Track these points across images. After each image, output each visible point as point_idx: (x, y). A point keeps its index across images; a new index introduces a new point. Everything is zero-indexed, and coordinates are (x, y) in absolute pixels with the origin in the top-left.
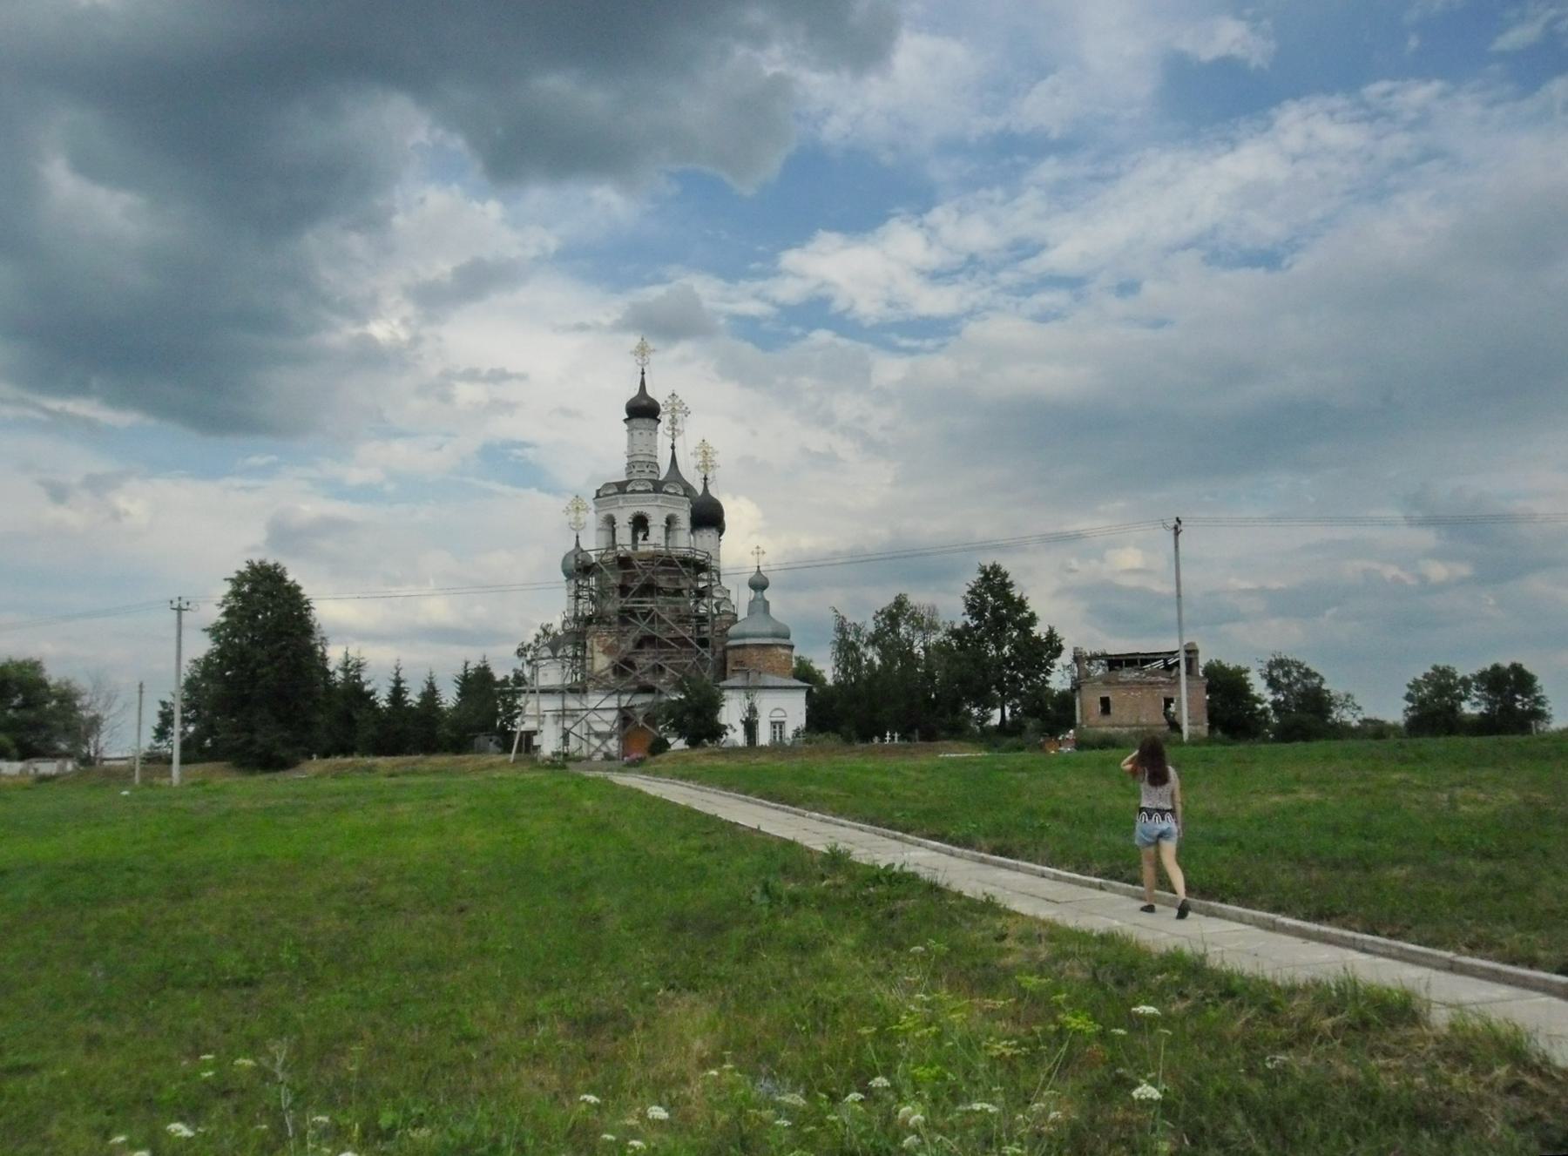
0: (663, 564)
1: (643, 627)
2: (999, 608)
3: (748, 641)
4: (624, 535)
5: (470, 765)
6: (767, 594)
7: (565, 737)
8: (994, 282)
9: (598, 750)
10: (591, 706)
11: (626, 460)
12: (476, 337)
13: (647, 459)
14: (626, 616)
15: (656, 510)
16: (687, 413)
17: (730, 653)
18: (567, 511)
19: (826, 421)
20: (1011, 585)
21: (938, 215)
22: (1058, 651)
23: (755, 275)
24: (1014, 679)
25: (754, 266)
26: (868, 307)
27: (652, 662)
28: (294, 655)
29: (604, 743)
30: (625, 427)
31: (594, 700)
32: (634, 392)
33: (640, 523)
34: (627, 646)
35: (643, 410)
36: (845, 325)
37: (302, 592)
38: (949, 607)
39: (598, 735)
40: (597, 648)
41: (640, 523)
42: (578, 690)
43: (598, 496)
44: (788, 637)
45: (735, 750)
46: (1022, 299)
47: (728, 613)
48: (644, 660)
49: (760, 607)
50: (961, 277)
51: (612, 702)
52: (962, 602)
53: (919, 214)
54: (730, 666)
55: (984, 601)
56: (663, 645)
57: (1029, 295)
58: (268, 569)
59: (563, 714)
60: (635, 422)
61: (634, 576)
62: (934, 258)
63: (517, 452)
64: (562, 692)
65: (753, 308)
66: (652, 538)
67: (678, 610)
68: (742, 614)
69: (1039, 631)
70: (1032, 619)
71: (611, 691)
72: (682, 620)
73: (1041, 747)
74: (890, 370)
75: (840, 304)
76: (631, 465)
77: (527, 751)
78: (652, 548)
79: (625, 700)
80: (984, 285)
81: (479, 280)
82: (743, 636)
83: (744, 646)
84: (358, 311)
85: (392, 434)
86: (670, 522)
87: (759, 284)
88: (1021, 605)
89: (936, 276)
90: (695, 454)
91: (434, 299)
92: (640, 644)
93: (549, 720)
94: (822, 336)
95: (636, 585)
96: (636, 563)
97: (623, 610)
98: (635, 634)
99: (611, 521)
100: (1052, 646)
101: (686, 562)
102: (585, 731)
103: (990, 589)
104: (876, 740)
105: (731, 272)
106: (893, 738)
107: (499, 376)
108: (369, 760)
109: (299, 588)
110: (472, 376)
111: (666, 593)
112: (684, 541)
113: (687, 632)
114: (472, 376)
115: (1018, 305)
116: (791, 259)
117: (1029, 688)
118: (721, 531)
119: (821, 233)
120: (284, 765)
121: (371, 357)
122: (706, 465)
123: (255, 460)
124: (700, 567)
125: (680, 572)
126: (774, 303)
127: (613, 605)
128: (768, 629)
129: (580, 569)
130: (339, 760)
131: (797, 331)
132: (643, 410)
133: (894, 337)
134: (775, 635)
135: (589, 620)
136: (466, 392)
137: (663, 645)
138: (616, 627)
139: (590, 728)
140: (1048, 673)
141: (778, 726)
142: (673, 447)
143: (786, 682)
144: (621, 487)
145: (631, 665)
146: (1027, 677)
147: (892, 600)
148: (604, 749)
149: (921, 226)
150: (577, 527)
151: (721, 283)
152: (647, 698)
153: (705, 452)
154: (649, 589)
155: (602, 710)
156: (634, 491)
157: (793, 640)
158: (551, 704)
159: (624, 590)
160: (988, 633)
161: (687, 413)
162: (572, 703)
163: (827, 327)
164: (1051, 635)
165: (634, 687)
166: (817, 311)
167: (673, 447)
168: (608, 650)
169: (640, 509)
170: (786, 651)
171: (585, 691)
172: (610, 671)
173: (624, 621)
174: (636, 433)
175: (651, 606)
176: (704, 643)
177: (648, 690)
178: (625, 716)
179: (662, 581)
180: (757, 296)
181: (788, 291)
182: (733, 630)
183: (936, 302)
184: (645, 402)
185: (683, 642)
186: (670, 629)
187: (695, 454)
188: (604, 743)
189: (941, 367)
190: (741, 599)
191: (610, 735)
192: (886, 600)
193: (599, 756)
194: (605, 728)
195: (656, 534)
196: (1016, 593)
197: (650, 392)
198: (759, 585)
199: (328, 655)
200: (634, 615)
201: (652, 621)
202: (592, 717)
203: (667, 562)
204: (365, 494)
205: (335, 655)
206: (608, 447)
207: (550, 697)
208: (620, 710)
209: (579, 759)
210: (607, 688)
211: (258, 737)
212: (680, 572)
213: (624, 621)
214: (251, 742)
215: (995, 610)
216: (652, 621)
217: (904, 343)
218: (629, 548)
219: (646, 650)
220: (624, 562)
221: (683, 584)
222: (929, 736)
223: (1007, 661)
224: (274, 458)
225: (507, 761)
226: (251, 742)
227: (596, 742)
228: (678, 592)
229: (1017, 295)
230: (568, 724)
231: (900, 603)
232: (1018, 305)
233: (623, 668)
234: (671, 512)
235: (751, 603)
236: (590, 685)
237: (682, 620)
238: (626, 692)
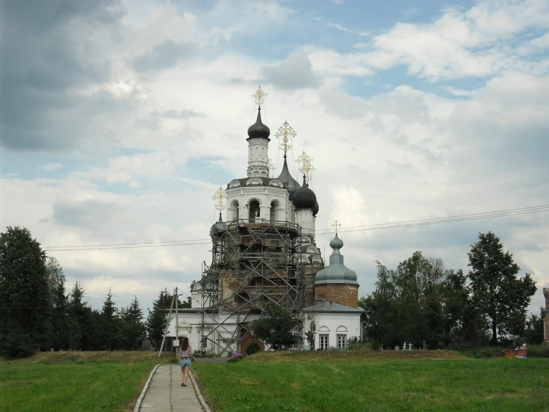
0: (267, 231)
1: (254, 272)
2: (493, 262)
3: (328, 281)
4: (244, 214)
5: (134, 357)
6: (342, 251)
7: (204, 340)
8: (515, 54)
9: (224, 350)
10: (220, 322)
11: (248, 165)
12: (173, 90)
13: (260, 164)
14: (244, 264)
15: (265, 197)
16: (294, 135)
17: (317, 289)
18: (214, 198)
19: (401, 141)
20: (501, 246)
21: (474, 12)
22: (533, 290)
23: (359, 51)
24: (503, 309)
25: (358, 45)
26: (433, 71)
27: (260, 294)
28: (32, 286)
29: (228, 346)
30: (247, 143)
31: (222, 318)
32: (253, 121)
33: (254, 206)
34: (245, 283)
35: (259, 133)
36: (419, 82)
37: (40, 246)
38: (457, 260)
39: (225, 341)
40: (225, 284)
41: (254, 206)
42: (212, 311)
43: (228, 188)
44: (355, 279)
45: (305, 352)
46: (534, 64)
47: (318, 263)
48: (256, 292)
49: (338, 259)
50: (492, 50)
51: (233, 320)
52: (468, 257)
53: (463, 11)
54: (316, 298)
55: (482, 257)
56: (266, 283)
57: (538, 61)
58: (20, 232)
59: (202, 327)
60: (253, 140)
61: (250, 239)
62: (475, 40)
63: (214, 162)
64: (202, 312)
65: (360, 71)
66: (262, 216)
67: (278, 261)
68: (327, 263)
69: (519, 276)
70: (515, 269)
71: (234, 313)
72: (280, 267)
73: (504, 355)
74: (442, 109)
75: (414, 69)
76: (250, 168)
77: (169, 350)
78: (260, 222)
79: (242, 318)
80: (508, 56)
81: (168, 55)
82: (326, 278)
83: (325, 285)
84: (99, 75)
85: (130, 152)
86: (274, 204)
87: (361, 57)
88: (508, 259)
89: (475, 51)
90: (299, 161)
91: (145, 66)
92: (253, 282)
93: (194, 330)
94: (404, 90)
95: (251, 244)
96: (250, 231)
97: (242, 261)
98: (249, 276)
99: (236, 204)
100: (528, 287)
101: (283, 230)
102: (217, 338)
103: (486, 249)
104: (397, 348)
105: (344, 47)
106: (408, 346)
107: (188, 114)
108: (75, 353)
109: (38, 244)
110: (171, 114)
111: (270, 250)
112: (283, 217)
113: (284, 275)
114: (171, 114)
115: (532, 68)
116: (381, 40)
117: (511, 314)
118: (315, 211)
119: (399, 25)
120: (26, 354)
121: (107, 104)
122: (307, 168)
123: (50, 167)
124: (294, 234)
125: (279, 237)
126: (372, 68)
127: (236, 256)
128: (342, 274)
129: (218, 234)
130: (62, 352)
131: (388, 86)
132: (259, 133)
133: (450, 89)
134: (346, 278)
135: (221, 266)
136: (171, 125)
137: (266, 283)
138: (237, 272)
139: (220, 335)
140: (526, 305)
141: (325, 338)
142: (285, 157)
143: (347, 309)
144: (243, 182)
145: (245, 295)
146: (511, 307)
147: (411, 256)
148: (229, 350)
149: (465, 19)
150: (220, 207)
151: (337, 55)
152: (256, 318)
153: (305, 160)
154: (258, 247)
155: (227, 325)
156: (250, 185)
157: (359, 281)
158: (195, 320)
159: (243, 248)
160: (485, 277)
161: (294, 135)
162: (208, 320)
163: (407, 84)
164: (528, 279)
165: (248, 310)
166: (398, 74)
167: (285, 157)
168: (232, 286)
169: (254, 197)
170: (353, 288)
171: (217, 312)
172: (233, 299)
173: (242, 267)
174: (254, 148)
175: (264, 258)
176: (293, 282)
177: (256, 312)
178: (242, 328)
179: (268, 243)
180: (360, 64)
181: (381, 60)
182: (319, 274)
183: (474, 67)
184: (260, 128)
185: (280, 282)
186: (272, 273)
187: (299, 161)
188: (228, 346)
189: (476, 108)
190: (327, 253)
191: (233, 341)
192: (407, 255)
193: (225, 354)
194: (229, 336)
195: (265, 213)
196: (504, 251)
197: (264, 121)
198: (337, 245)
199: (64, 286)
200: (248, 264)
201: (260, 267)
202: (221, 329)
203: (271, 230)
204: (120, 188)
205: (69, 288)
206: (238, 157)
207: (194, 315)
208: (239, 324)
209: (211, 356)
210: (230, 310)
211: (9, 337)
212: (279, 237)
213: (242, 267)
214: (5, 340)
215: (490, 262)
216: (260, 267)
217: (458, 93)
218: (246, 222)
219: (257, 286)
220: (243, 230)
221: (282, 245)
222: (433, 345)
223: (497, 296)
224: (59, 166)
225: (156, 356)
226: (5, 340)
227: (224, 345)
228: (278, 249)
229: (532, 61)
230: (206, 333)
231: (416, 258)
232: (532, 68)
233: (241, 297)
234: (274, 198)
235: (331, 257)
236: (220, 308)
237: (280, 267)
238: (243, 313)
